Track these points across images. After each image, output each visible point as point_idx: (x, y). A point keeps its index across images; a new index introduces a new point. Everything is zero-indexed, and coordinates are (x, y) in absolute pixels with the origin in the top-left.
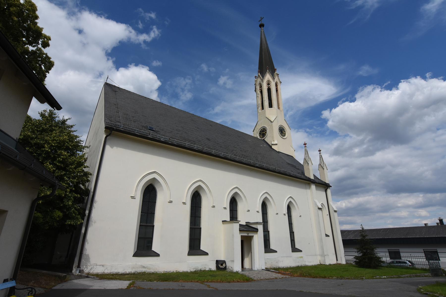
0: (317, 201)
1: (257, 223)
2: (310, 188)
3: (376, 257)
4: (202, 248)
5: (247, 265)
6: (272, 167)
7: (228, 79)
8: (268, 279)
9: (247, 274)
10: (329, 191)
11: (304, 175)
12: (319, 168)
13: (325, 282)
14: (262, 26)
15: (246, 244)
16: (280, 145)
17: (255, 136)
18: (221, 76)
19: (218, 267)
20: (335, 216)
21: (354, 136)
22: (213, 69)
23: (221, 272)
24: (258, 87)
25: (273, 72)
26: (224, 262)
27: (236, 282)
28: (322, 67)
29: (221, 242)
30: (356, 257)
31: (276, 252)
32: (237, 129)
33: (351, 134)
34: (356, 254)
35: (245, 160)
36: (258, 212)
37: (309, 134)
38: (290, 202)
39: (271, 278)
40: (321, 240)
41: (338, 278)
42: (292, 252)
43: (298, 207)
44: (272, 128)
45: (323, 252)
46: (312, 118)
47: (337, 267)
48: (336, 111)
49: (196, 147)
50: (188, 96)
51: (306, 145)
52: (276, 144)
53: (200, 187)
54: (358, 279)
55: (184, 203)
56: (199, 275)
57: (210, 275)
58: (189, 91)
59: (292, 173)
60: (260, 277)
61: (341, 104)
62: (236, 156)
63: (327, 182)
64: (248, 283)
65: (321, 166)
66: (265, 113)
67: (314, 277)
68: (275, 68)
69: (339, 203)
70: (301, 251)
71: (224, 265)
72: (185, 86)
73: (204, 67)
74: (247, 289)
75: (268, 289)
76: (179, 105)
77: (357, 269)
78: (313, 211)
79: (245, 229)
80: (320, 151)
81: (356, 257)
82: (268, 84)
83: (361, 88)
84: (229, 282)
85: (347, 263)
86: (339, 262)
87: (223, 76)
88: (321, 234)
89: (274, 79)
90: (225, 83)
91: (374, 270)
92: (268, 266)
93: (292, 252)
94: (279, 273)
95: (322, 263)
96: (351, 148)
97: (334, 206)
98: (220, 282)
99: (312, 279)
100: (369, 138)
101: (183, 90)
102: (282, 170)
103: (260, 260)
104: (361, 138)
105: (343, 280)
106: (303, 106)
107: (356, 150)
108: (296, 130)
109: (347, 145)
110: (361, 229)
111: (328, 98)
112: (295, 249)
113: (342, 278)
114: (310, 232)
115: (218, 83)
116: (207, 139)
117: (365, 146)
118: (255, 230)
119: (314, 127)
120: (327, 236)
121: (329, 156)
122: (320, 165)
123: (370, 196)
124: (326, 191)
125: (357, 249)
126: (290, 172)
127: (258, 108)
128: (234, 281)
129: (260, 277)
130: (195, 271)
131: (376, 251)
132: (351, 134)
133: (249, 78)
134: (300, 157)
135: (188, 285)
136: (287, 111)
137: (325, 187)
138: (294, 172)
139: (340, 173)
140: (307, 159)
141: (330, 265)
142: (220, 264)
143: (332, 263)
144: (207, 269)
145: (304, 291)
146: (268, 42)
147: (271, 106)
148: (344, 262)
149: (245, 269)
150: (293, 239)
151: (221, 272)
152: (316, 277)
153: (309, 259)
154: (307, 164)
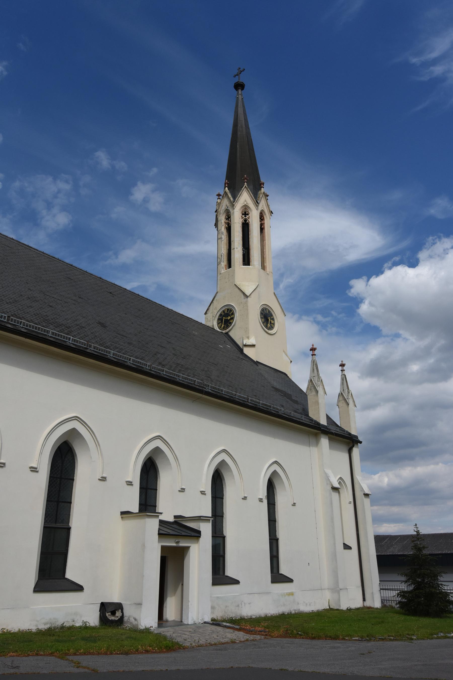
0: (329, 472)
1: (199, 519)
2: (317, 443)
3: (441, 593)
4: (70, 574)
5: (171, 614)
6: (240, 395)
7: (154, 191)
8: (215, 644)
9: (168, 634)
10: (356, 451)
11: (307, 415)
12: (339, 401)
13: (334, 648)
14: (239, 86)
15: (172, 564)
16: (259, 346)
17: (209, 324)
18: (139, 183)
19: (103, 619)
20: (365, 505)
21: (413, 339)
22: (121, 165)
23: (111, 631)
24: (222, 219)
25: (256, 188)
26: (119, 606)
27: (142, 653)
28: (358, 191)
29: (112, 560)
30: (402, 594)
31: (237, 582)
32: (170, 307)
33: (404, 333)
34: (404, 587)
35: (181, 377)
36: (203, 493)
37: (323, 326)
38: (275, 472)
39: (223, 641)
40: (334, 557)
41: (362, 639)
42: (273, 582)
43: (290, 484)
44: (247, 310)
45: (337, 583)
46: (330, 294)
47: (364, 613)
48: (377, 281)
49: (70, 341)
50: (62, 220)
51: (316, 352)
52: (253, 346)
53: (74, 432)
54: (401, 640)
55: (34, 470)
56: (58, 639)
57: (83, 639)
58: (64, 209)
59: (282, 411)
60: (197, 639)
61: (390, 268)
62: (163, 366)
63: (353, 432)
64: (169, 655)
65: (344, 397)
66: (233, 276)
67: (314, 638)
68: (262, 180)
69: (376, 477)
70: (291, 581)
71: (118, 614)
72: (55, 197)
73: (103, 159)
74: (164, 668)
75: (213, 667)
76: (37, 240)
77: (403, 617)
78: (320, 492)
79: (172, 532)
80: (342, 365)
81: (402, 594)
82: (245, 214)
83: (431, 238)
84: (127, 654)
85: (384, 606)
86: (368, 603)
87: (144, 183)
88: (335, 544)
89: (257, 203)
90: (146, 200)
91: (436, 620)
92: (218, 615)
93: (273, 582)
94: (239, 630)
95: (334, 606)
96: (405, 362)
97: (365, 483)
98: (106, 654)
99: (308, 641)
100: (442, 342)
101: (49, 206)
102: (262, 402)
103: (200, 601)
104: (426, 342)
105: (372, 643)
106: (312, 265)
107: (415, 367)
108: (296, 316)
109: (397, 355)
110: (415, 533)
111: (364, 257)
112: (278, 577)
113: (370, 638)
114: (310, 539)
115: (132, 198)
116: (100, 323)
117: (431, 361)
118: (193, 534)
119: (334, 313)
120: (347, 547)
121: (359, 377)
122: (341, 395)
123: (437, 464)
124: (350, 452)
125: (406, 575)
126: (280, 407)
127: (218, 264)
128: (137, 650)
129: (197, 639)
130: (49, 629)
131: (441, 579)
132: (404, 333)
133: (210, 198)
134: (300, 377)
135: (28, 664)
136: (282, 275)
137: (348, 444)
138: (287, 409)
139: (381, 413)
140: (315, 380)
141: (349, 610)
142: (110, 612)
143: (353, 607)
144: (78, 624)
145: (290, 669)
146: (250, 126)
147: (246, 261)
148: (377, 604)
149: (167, 621)
150: (275, 554)
151: (110, 630)
152: (319, 638)
153: (307, 597)
154: (314, 393)
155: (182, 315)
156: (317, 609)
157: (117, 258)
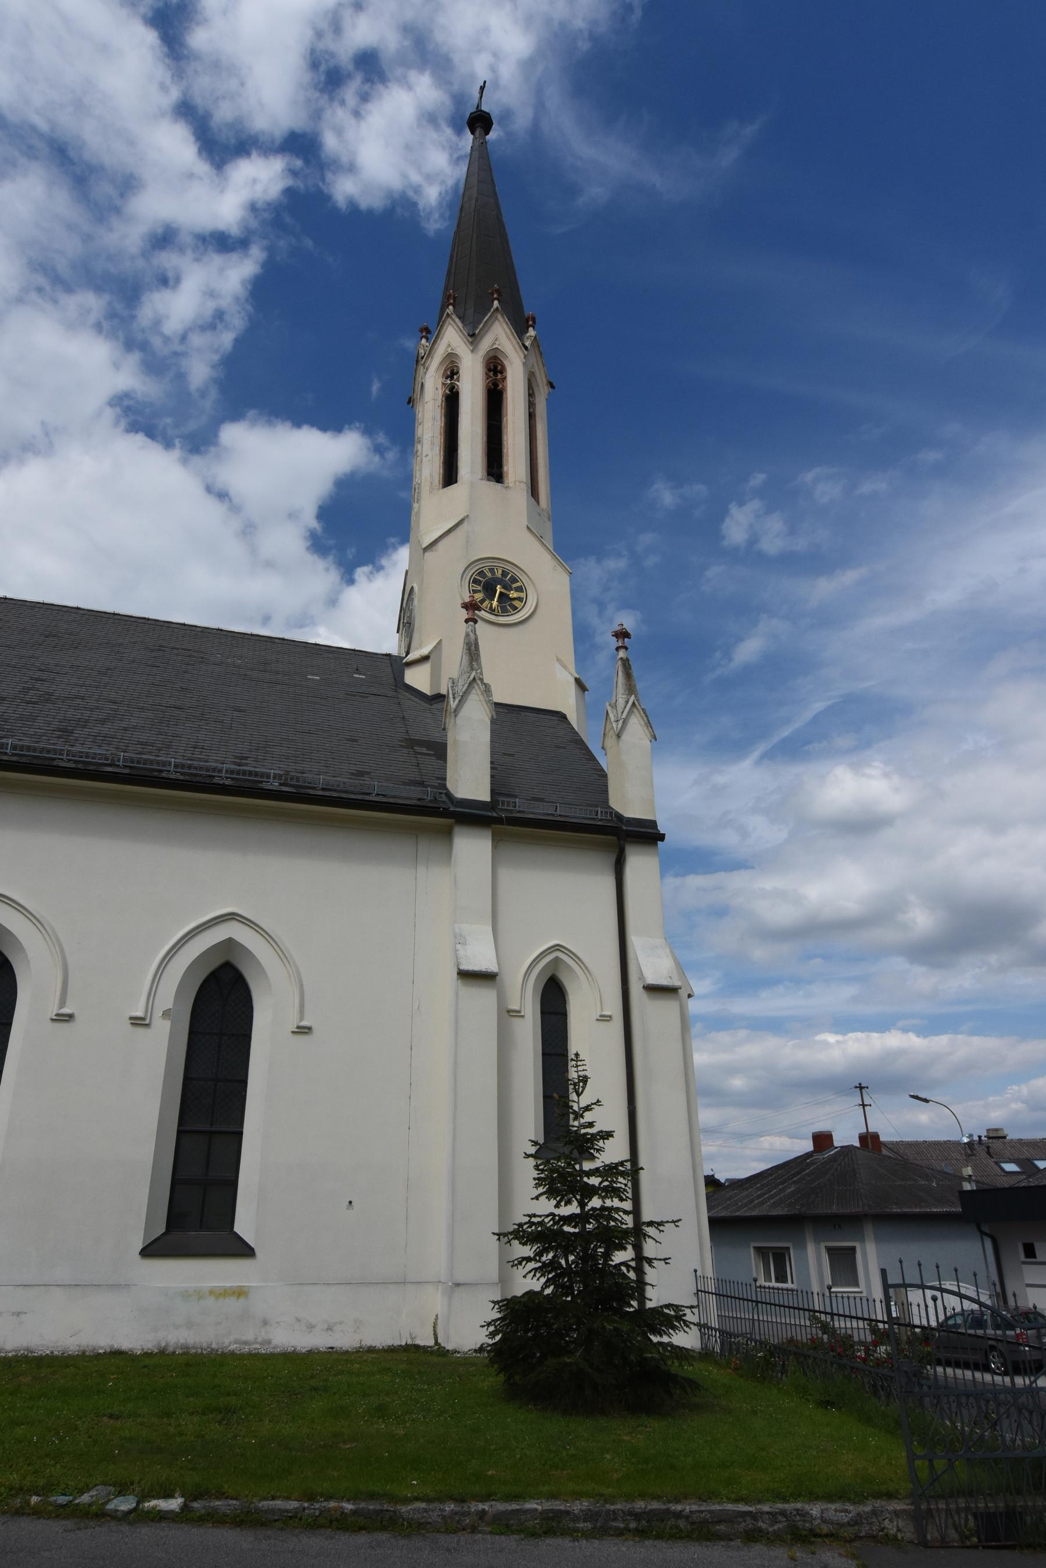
87: (741, 503)
155: (114, 614)
156: (25, 1345)
157: (731, 660)
